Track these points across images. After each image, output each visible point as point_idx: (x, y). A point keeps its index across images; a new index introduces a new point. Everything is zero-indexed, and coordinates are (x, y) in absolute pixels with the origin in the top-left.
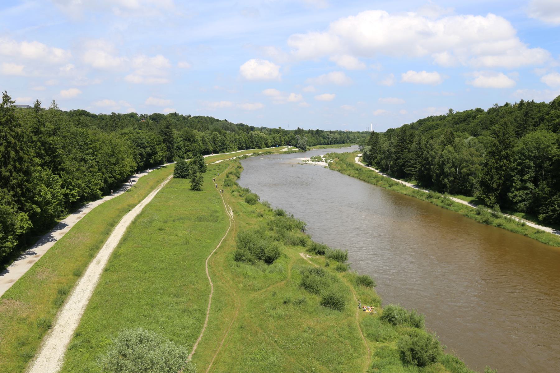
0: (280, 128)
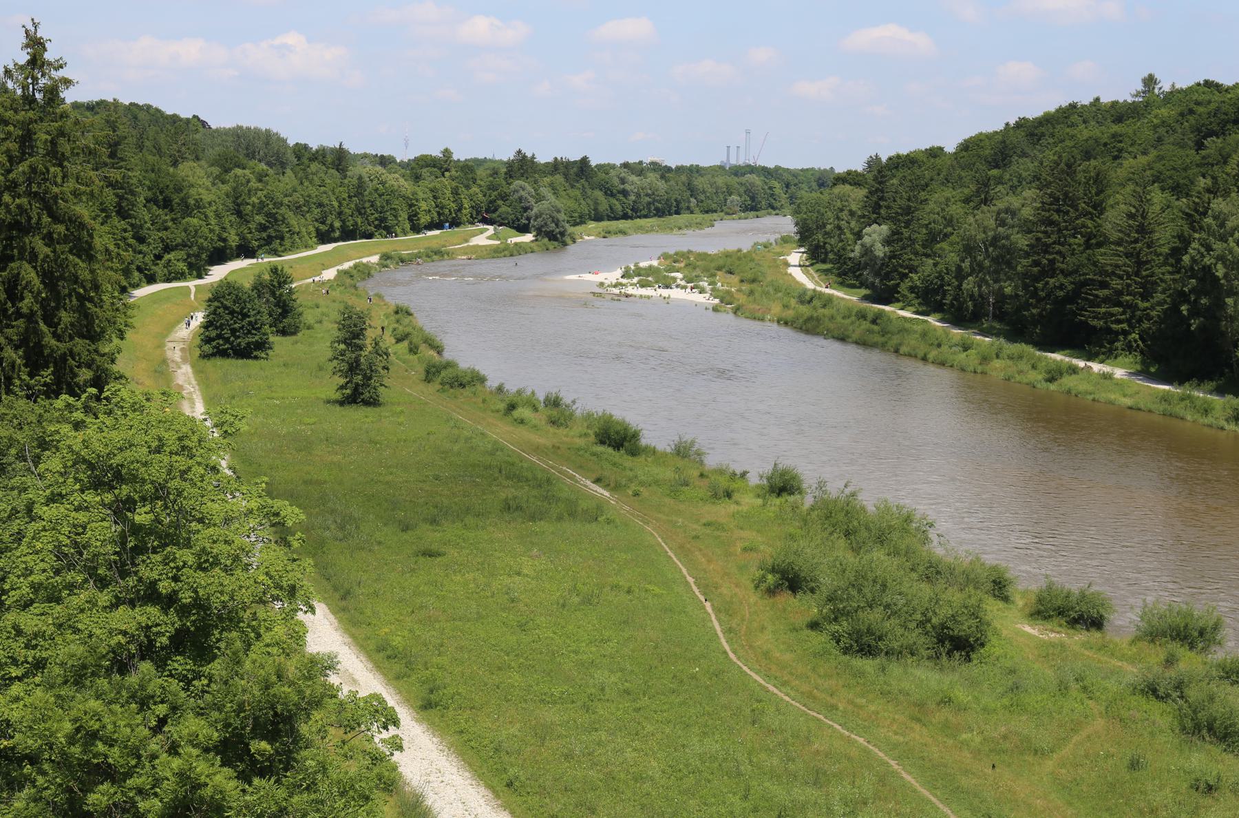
0: (447, 152)
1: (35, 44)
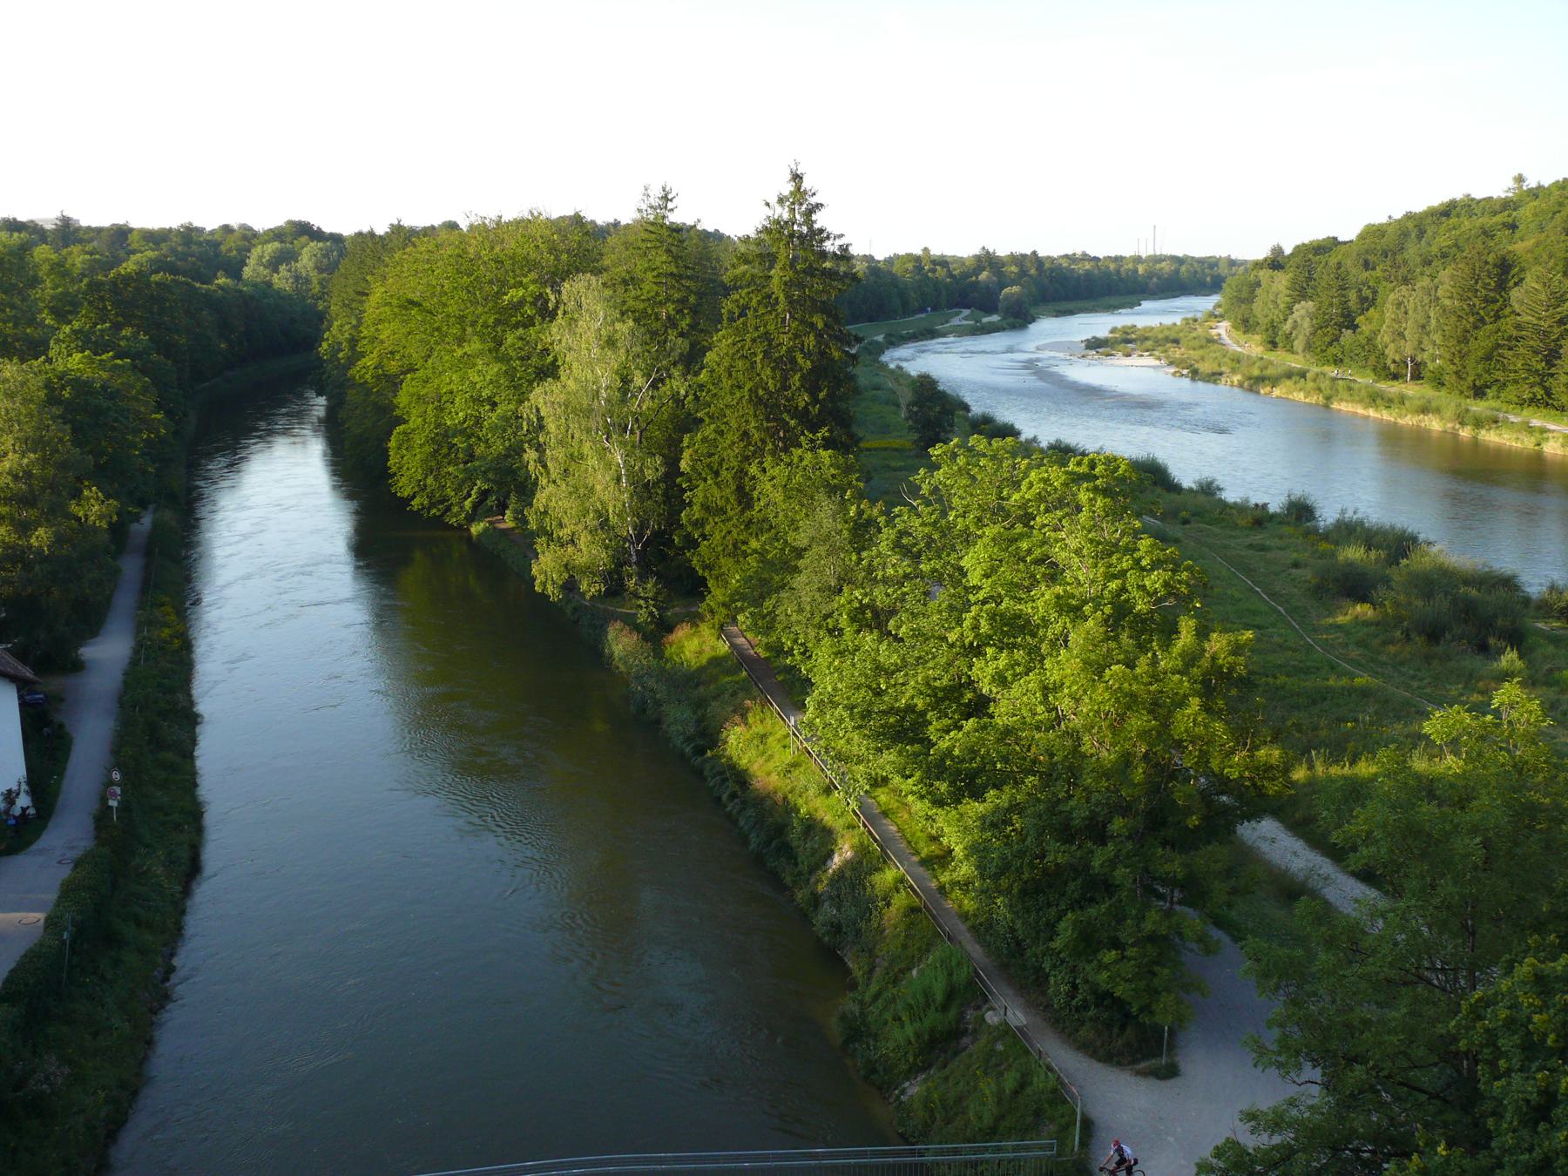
1: (797, 178)
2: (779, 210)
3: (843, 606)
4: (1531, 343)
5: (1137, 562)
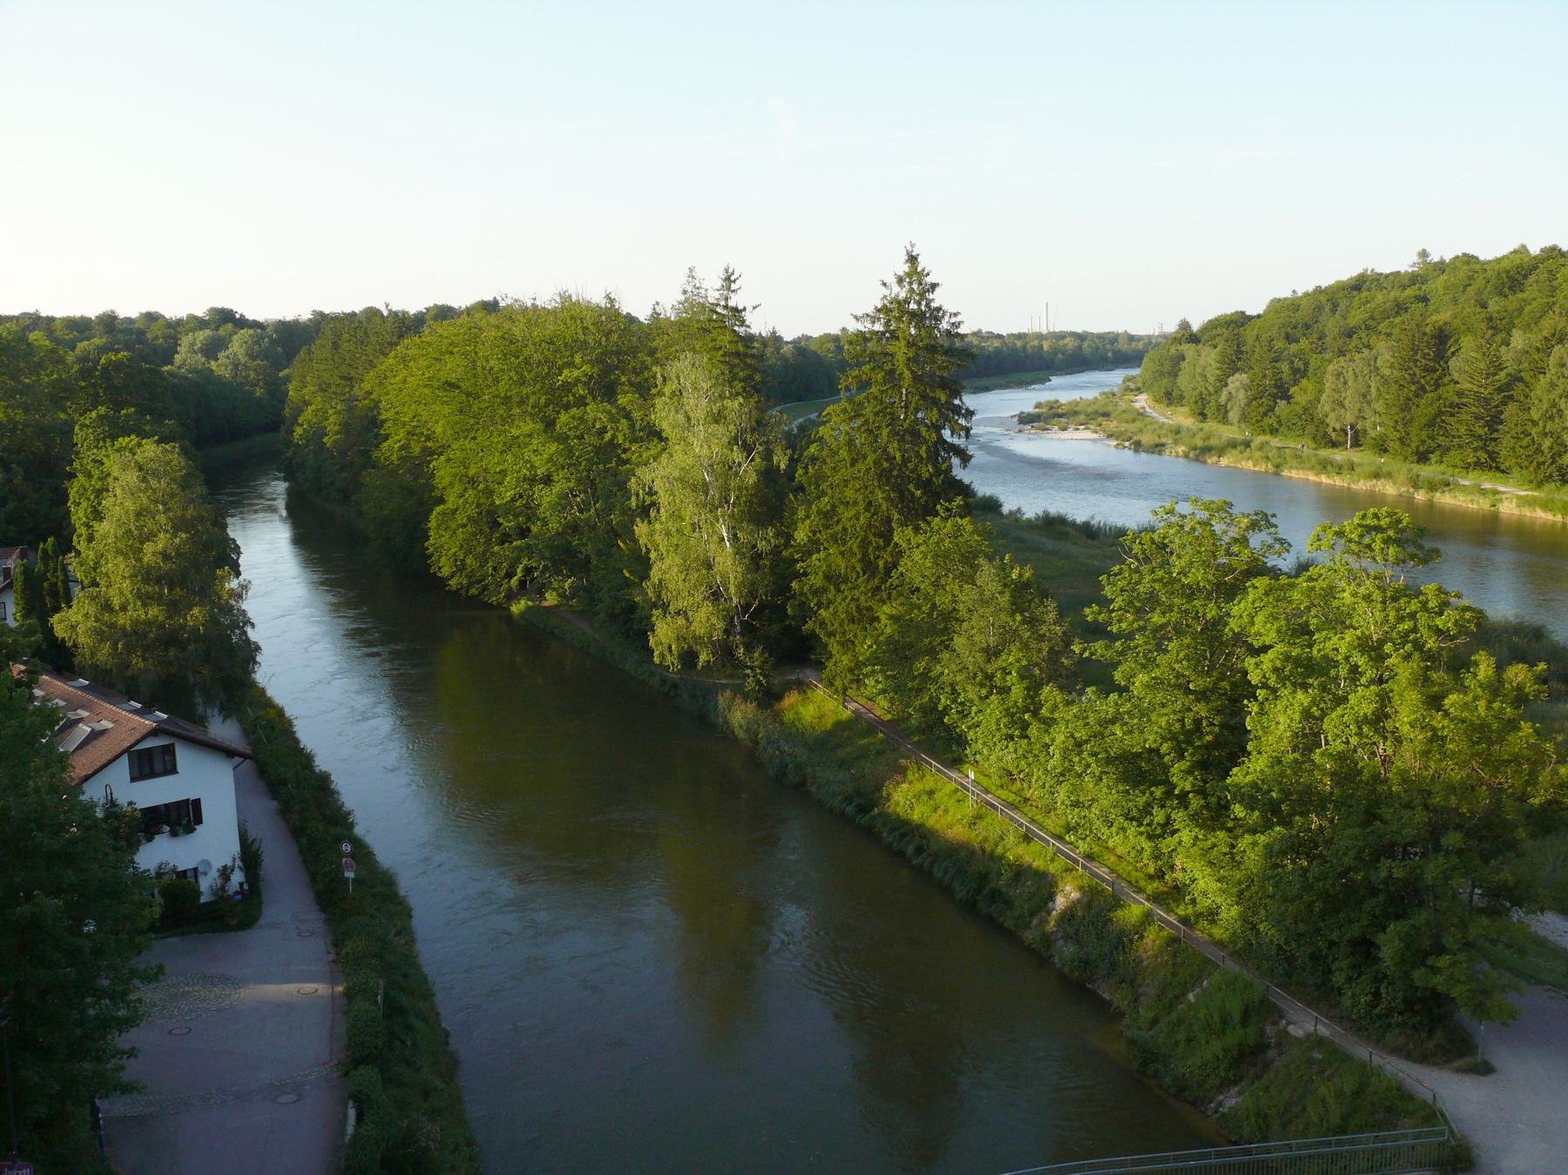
1: (913, 259)
2: (896, 289)
3: (1011, 664)
4: (1474, 409)
5: (1424, 604)
